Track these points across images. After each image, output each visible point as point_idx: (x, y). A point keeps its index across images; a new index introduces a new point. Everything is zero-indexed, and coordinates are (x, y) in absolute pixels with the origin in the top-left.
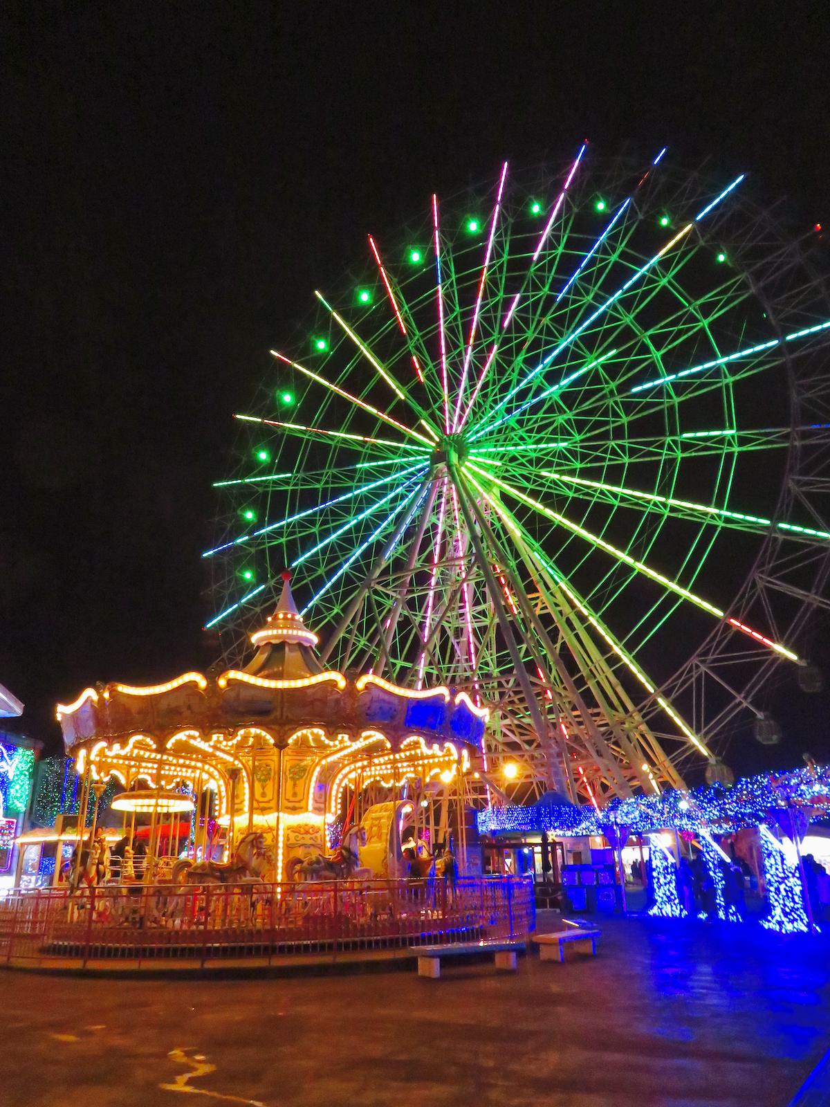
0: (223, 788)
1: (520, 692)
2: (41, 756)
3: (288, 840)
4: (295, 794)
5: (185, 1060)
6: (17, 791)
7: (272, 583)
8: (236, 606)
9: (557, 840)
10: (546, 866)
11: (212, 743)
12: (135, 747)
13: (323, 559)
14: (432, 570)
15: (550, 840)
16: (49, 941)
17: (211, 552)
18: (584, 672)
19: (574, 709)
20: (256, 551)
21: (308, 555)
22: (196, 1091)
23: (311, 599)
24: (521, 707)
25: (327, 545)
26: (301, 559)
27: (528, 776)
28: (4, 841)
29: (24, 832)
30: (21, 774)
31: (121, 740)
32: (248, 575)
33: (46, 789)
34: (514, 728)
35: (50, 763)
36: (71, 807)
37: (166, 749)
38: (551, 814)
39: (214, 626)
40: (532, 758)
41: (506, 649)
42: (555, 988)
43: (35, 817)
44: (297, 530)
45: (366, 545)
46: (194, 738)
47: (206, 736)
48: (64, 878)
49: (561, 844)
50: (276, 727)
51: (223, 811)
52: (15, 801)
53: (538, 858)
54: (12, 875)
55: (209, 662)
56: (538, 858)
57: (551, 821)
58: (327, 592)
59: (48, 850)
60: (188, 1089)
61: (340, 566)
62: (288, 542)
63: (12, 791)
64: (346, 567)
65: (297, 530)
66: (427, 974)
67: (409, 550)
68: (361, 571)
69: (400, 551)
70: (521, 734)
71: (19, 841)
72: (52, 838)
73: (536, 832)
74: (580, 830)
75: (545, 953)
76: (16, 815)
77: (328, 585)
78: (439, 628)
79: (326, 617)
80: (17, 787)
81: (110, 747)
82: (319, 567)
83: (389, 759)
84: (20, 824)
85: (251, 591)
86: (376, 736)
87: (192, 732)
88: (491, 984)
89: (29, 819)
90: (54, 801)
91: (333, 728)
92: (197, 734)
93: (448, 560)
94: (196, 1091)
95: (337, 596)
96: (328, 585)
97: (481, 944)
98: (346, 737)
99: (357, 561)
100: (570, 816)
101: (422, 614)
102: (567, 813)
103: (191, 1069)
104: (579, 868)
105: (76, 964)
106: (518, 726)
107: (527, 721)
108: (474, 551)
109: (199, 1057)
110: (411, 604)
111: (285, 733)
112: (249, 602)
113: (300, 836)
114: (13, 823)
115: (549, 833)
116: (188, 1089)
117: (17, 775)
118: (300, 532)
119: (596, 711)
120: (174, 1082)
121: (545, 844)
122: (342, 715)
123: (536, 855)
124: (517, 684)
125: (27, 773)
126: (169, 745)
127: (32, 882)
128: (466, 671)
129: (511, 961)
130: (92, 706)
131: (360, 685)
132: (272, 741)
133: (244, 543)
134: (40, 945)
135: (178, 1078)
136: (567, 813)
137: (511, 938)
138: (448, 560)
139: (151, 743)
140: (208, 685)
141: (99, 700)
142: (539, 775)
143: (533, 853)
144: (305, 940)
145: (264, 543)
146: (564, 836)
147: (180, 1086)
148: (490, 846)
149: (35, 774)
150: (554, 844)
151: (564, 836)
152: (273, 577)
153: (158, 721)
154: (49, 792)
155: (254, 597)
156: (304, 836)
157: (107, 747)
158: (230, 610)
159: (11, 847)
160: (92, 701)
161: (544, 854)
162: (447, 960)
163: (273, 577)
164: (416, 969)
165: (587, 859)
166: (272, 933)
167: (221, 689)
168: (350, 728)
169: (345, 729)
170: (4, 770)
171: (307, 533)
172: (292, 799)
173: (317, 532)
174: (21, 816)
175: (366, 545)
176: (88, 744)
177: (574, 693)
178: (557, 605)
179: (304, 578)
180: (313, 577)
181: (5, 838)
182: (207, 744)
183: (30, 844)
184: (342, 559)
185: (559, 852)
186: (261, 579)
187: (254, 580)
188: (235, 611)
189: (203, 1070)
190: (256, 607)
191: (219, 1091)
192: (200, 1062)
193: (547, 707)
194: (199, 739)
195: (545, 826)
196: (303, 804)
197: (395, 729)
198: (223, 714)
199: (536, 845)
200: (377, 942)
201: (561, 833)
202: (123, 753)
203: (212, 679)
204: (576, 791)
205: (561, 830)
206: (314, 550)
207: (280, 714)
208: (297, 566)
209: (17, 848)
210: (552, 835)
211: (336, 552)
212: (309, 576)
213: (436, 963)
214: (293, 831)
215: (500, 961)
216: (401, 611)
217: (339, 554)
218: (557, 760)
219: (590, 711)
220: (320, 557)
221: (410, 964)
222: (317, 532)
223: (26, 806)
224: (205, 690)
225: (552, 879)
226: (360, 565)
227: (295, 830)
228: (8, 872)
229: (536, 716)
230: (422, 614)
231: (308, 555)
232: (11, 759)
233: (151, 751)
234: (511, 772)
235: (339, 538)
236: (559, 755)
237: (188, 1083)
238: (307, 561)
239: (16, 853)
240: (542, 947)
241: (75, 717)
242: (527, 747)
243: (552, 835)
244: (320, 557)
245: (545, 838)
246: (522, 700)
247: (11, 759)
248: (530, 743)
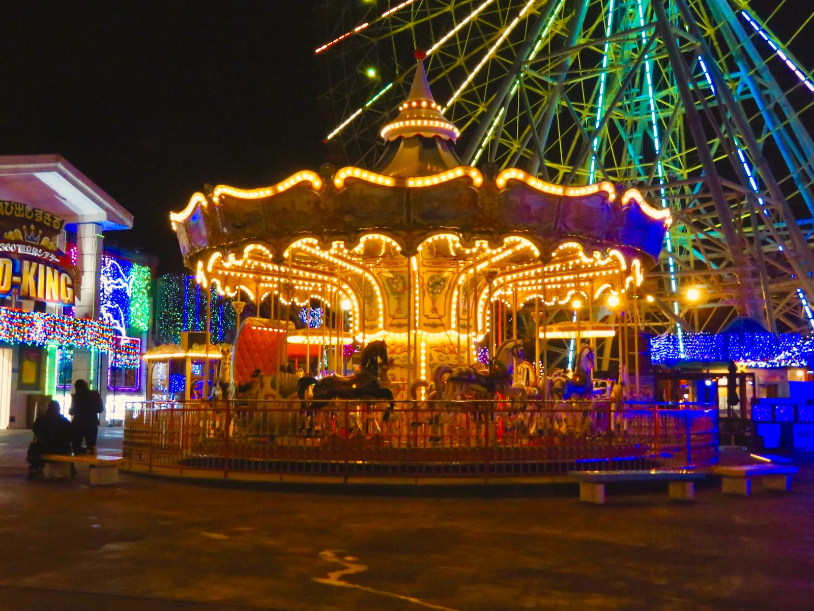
0: (357, 309)
1: (709, 199)
2: (156, 275)
3: (431, 358)
4: (435, 310)
5: (335, 560)
6: (137, 310)
7: (401, 80)
8: (360, 111)
9: (746, 371)
10: (732, 399)
11: (332, 251)
12: (251, 258)
13: (462, 45)
14: (602, 48)
15: (739, 371)
16: (188, 453)
17: (324, 47)
18: (794, 174)
19: (778, 220)
20: (380, 42)
21: (443, 40)
22: (350, 585)
23: (451, 96)
24: (708, 218)
25: (466, 27)
26: (436, 47)
27: (716, 301)
28: (131, 361)
29: (149, 348)
30: (139, 291)
31: (235, 249)
32: (371, 73)
33: (167, 307)
34: (698, 244)
35: (168, 281)
36: (195, 327)
37: (284, 259)
38: (742, 342)
39: (336, 137)
40: (720, 279)
41: (694, 146)
42: (738, 519)
43: (159, 335)
44: (428, 10)
45: (515, 22)
46: (312, 246)
47: (325, 246)
48: (196, 396)
49: (752, 375)
50: (403, 233)
51: (357, 328)
52: (137, 320)
53: (723, 393)
54: (142, 394)
55: (325, 160)
56: (723, 393)
57: (741, 350)
58: (470, 86)
59: (176, 368)
60: (342, 584)
61: (485, 51)
62: (416, 27)
63: (132, 309)
64: (492, 51)
65: (428, 10)
66: (589, 499)
67: (571, 26)
68: (512, 58)
69: (559, 27)
70: (708, 251)
71: (147, 357)
72: (180, 354)
73: (722, 363)
74: (780, 359)
75: (727, 487)
76: (139, 334)
77: (471, 77)
78: (608, 120)
79: (470, 117)
80: (137, 305)
81: (225, 257)
82: (458, 55)
83: (537, 274)
84: (145, 343)
85: (376, 93)
86: (525, 243)
87: (311, 240)
88: (662, 512)
89: (153, 338)
90: (178, 321)
91: (469, 232)
92: (315, 241)
93: (622, 33)
94: (350, 585)
95: (481, 91)
96: (471, 77)
97: (653, 472)
98: (485, 244)
99: (505, 43)
100: (765, 345)
101: (590, 105)
102: (762, 342)
103: (342, 568)
104: (772, 401)
105: (218, 475)
106: (704, 242)
107: (716, 235)
108: (655, 19)
109: (349, 558)
110: (575, 94)
111: (414, 239)
112: (375, 105)
113: (444, 356)
114: (137, 342)
115: (738, 364)
116: (342, 584)
117: (135, 293)
118: (432, 13)
119: (806, 222)
120: (327, 577)
121: (732, 376)
122: (482, 216)
123: (720, 390)
124: (705, 189)
125: (146, 291)
126: (286, 254)
127: (163, 401)
128: (639, 175)
129: (688, 491)
130: (202, 212)
131: (501, 181)
132: (399, 249)
133: (362, 31)
134: (180, 458)
135: (331, 575)
136: (762, 342)
137: (688, 469)
138: (622, 33)
139: (267, 252)
140: (323, 185)
141: (209, 205)
142: (727, 298)
143: (715, 386)
144: (454, 461)
145: (388, 31)
146: (757, 367)
147: (333, 580)
148: (666, 376)
149: (153, 293)
150: (743, 376)
151: (757, 367)
152: (401, 73)
153: (274, 226)
154: (171, 311)
155: (381, 99)
156: (450, 355)
157: (223, 258)
158: (353, 117)
159: (138, 366)
160: (202, 207)
161: (731, 387)
162: (612, 487)
163: (401, 73)
164: (577, 494)
165: (784, 392)
166: (414, 453)
167: (338, 190)
168: (491, 234)
169: (483, 235)
170: (122, 287)
171: (440, 13)
172: (431, 315)
173: (452, 11)
174: (145, 336)
175: (515, 22)
176: (204, 255)
177: (779, 199)
178: (763, 87)
179: (441, 71)
180: (451, 69)
181: (131, 357)
182: (326, 253)
183: (157, 361)
184: (487, 43)
185: (749, 383)
186: (386, 76)
187: (379, 79)
188: (359, 116)
189: (354, 569)
190: (383, 110)
191: (373, 587)
192: (351, 562)
193: (743, 217)
194: (318, 248)
195: (733, 355)
196: (444, 320)
197: (547, 234)
198: (340, 218)
199: (721, 376)
200: (533, 466)
201: (753, 363)
202: (240, 263)
203: (327, 178)
204: (775, 318)
205: (754, 360)
206: (451, 34)
207: (410, 217)
208: (431, 54)
209: (144, 366)
210: (742, 366)
211: (479, 34)
212: (447, 68)
213: (600, 489)
214: (437, 351)
215: (674, 491)
216: (560, 102)
217: (483, 37)
218: (752, 281)
219: (799, 223)
220: (458, 43)
221: (572, 490)
222: (452, 11)
223: (148, 325)
224: (320, 191)
225: (739, 416)
226: (510, 49)
227: (439, 349)
228: (138, 391)
229: (728, 229)
230: (590, 105)
231: (443, 40)
232: (127, 276)
233: (266, 261)
234: (694, 295)
235: (480, 15)
236: (755, 275)
237: (341, 578)
238: (442, 48)
239: (144, 372)
240: (725, 480)
241: (185, 224)
242: (714, 267)
243: (742, 366)
244: (458, 43)
245: (733, 368)
246: (709, 210)
247: (127, 276)
248: (718, 262)
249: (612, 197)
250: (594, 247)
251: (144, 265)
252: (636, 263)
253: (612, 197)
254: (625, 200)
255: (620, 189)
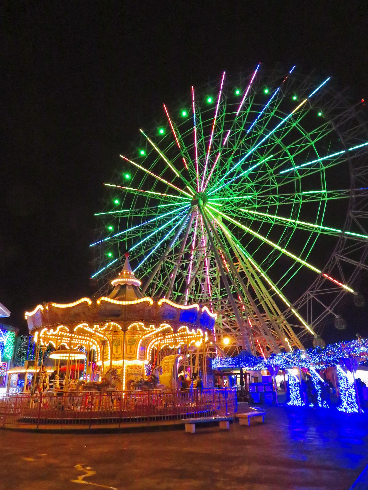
0: (99, 349)
1: (231, 306)
2: (18, 335)
3: (128, 372)
4: (131, 352)
5: (82, 469)
6: (7, 350)
7: (121, 258)
8: (104, 268)
9: (247, 372)
10: (242, 383)
11: (94, 329)
12: (60, 331)
13: (143, 248)
14: (191, 252)
15: (244, 372)
16: (22, 417)
17: (94, 245)
18: (259, 297)
19: (255, 314)
20: (114, 244)
21: (137, 246)
22: (87, 483)
23: (138, 265)
24: (231, 313)
25: (145, 241)
26: (134, 248)
27: (234, 344)
28: (2, 372)
29: (10, 368)
30: (9, 342)
31: (53, 328)
32: (110, 255)
33: (21, 349)
34: (228, 322)
35: (22, 338)
36: (32, 357)
37: (74, 332)
38: (244, 360)
39: (95, 277)
40: (236, 335)
41: (224, 287)
43: (16, 362)
44: (132, 234)
45: (162, 241)
46: (86, 327)
47: (91, 326)
48: (29, 389)
49: (249, 373)
50: (123, 322)
51: (99, 359)
52: (7, 354)
53: (239, 380)
55: (93, 293)
56: (239, 380)
57: (244, 363)
58: (145, 262)
59: (21, 376)
60: (83, 482)
61: (151, 251)
62: (128, 240)
63: (5, 350)
64: (153, 251)
65: (132, 234)
66: (189, 431)
67: (182, 244)
68: (160, 253)
69: (177, 244)
70: (231, 325)
71: (8, 372)
72: (23, 371)
73: (238, 368)
75: (242, 422)
76: (7, 361)
77: (146, 259)
78: (195, 278)
79: (144, 273)
80: (8, 348)
81: (49, 331)
82: (142, 251)
84: (9, 365)
85: (111, 262)
86: (167, 326)
87: (85, 324)
88: (218, 436)
89: (13, 362)
90: (24, 355)
91: (147, 322)
92: (87, 325)
93: (199, 248)
94: (87, 483)
95: (149, 264)
96: (146, 259)
97: (213, 418)
98: (153, 326)
99: (158, 248)
100: (253, 361)
102: (252, 360)
103: (85, 473)
104: (257, 384)
105: (34, 427)
106: (230, 321)
107: (234, 319)
108: (210, 244)
109: (88, 468)
110: (182, 267)
111: (126, 325)
112: (110, 267)
113: (133, 370)
114: (6, 364)
115: (243, 369)
116: (83, 482)
117: (8, 343)
118: (133, 236)
119: (264, 315)
120: (77, 479)
121: (241, 374)
122: (151, 317)
123: (238, 379)
124: (229, 303)
125: (12, 342)
126: (75, 330)
127: (14, 391)
128: (206, 297)
131: (160, 303)
132: (121, 328)
133: (108, 240)
134: (18, 418)
135: (79, 477)
136: (252, 360)
137: (227, 415)
138: (199, 248)
139: (67, 329)
140: (92, 303)
142: (239, 343)
143: (236, 377)
144: (135, 416)
145: (117, 240)
146: (250, 370)
147: (80, 480)
148: (217, 375)
149: (15, 343)
150: (246, 374)
151: (250, 370)
152: (121, 255)
153: (70, 319)
154: (22, 350)
155: (113, 264)
156: (135, 370)
157: (47, 331)
158: (102, 270)
159: (5, 375)
161: (241, 378)
162: (198, 425)
163: (121, 255)
164: (184, 429)
165: (260, 380)
166: (120, 413)
167: (98, 305)
168: (155, 322)
169: (153, 323)
170: (2, 341)
171: (136, 236)
172: (129, 354)
173: (141, 236)
174: (9, 361)
175: (162, 241)
176: (39, 329)
177: (254, 307)
178: (247, 268)
179: (135, 256)
180: (139, 255)
181: (2, 371)
182: (92, 329)
183: (13, 373)
184: (152, 248)
185: (248, 377)
186: (116, 256)
187: (113, 257)
188: (104, 270)
189: (90, 473)
190: (113, 269)
191: (97, 483)
192: (89, 470)
193: (242, 313)
194: (88, 327)
195: (242, 365)
196: (134, 356)
197: (175, 323)
198: (99, 316)
199: (238, 374)
200: (167, 417)
201: (249, 369)
202: (54, 333)
203: (94, 301)
204: (255, 350)
205: (249, 367)
206: (139, 244)
207: (124, 316)
208: (132, 250)
209: (7, 375)
210: (245, 370)
211: (149, 244)
212: (137, 255)
213: (193, 426)
214: (130, 368)
215: (222, 426)
216: (178, 270)
217: (150, 245)
218: (247, 337)
219: (262, 315)
220: (142, 247)
221: (182, 427)
222: (141, 236)
223: (11, 357)
224: (91, 305)
225: (245, 389)
226: (160, 250)
227: (131, 367)
229: (237, 317)
231: (137, 246)
232: (5, 336)
233: (67, 332)
234: (227, 342)
235: (150, 238)
236: (248, 334)
237: (84, 479)
238: (136, 248)
239: (7, 378)
242: (234, 331)
243: (245, 370)
244: (142, 247)
245: (242, 371)
246: (231, 310)
247: (5, 336)
248: (235, 329)
249: (198, 309)
250: (192, 328)
251: (12, 331)
252: (206, 333)
253: (198, 309)
254: (203, 310)
255: (201, 307)
